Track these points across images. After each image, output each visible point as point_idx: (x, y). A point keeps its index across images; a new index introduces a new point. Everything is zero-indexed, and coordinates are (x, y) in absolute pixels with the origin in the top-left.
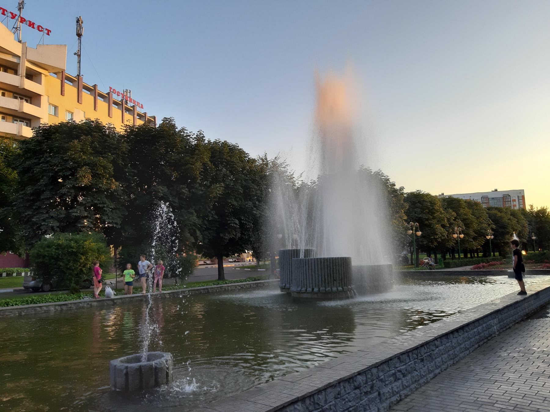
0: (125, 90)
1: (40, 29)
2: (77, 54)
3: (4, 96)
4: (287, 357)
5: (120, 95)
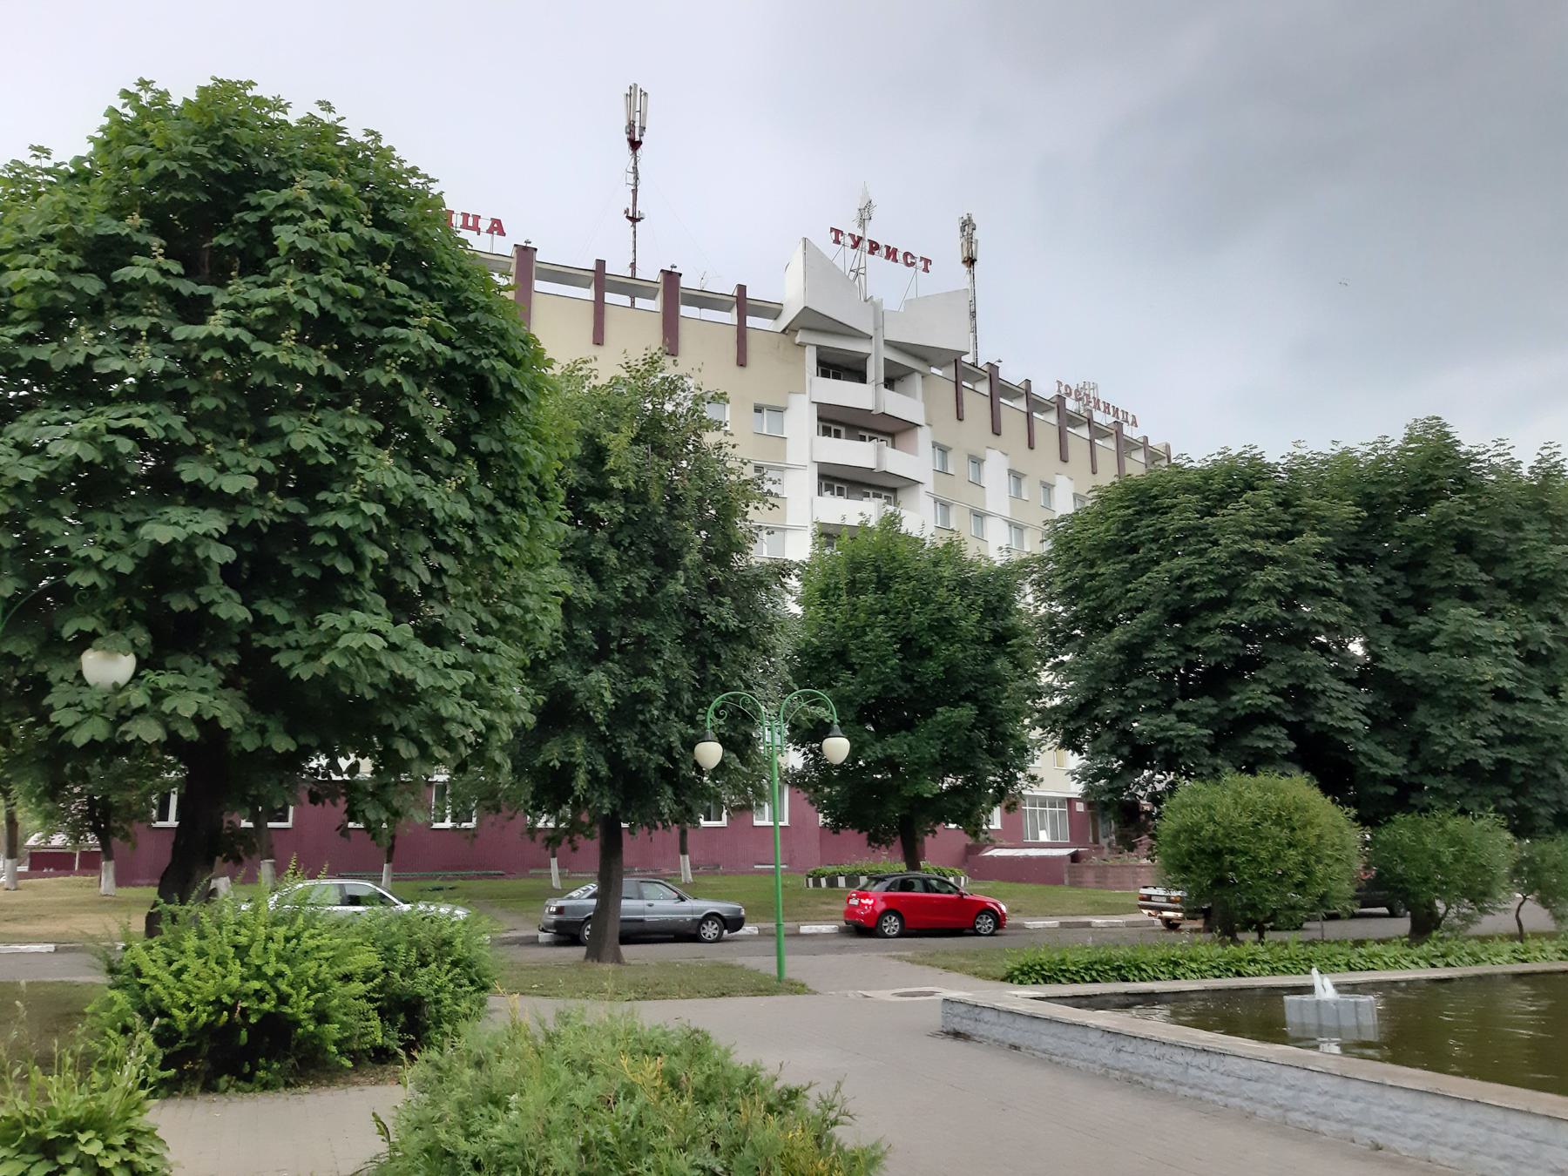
4: (504, 944)
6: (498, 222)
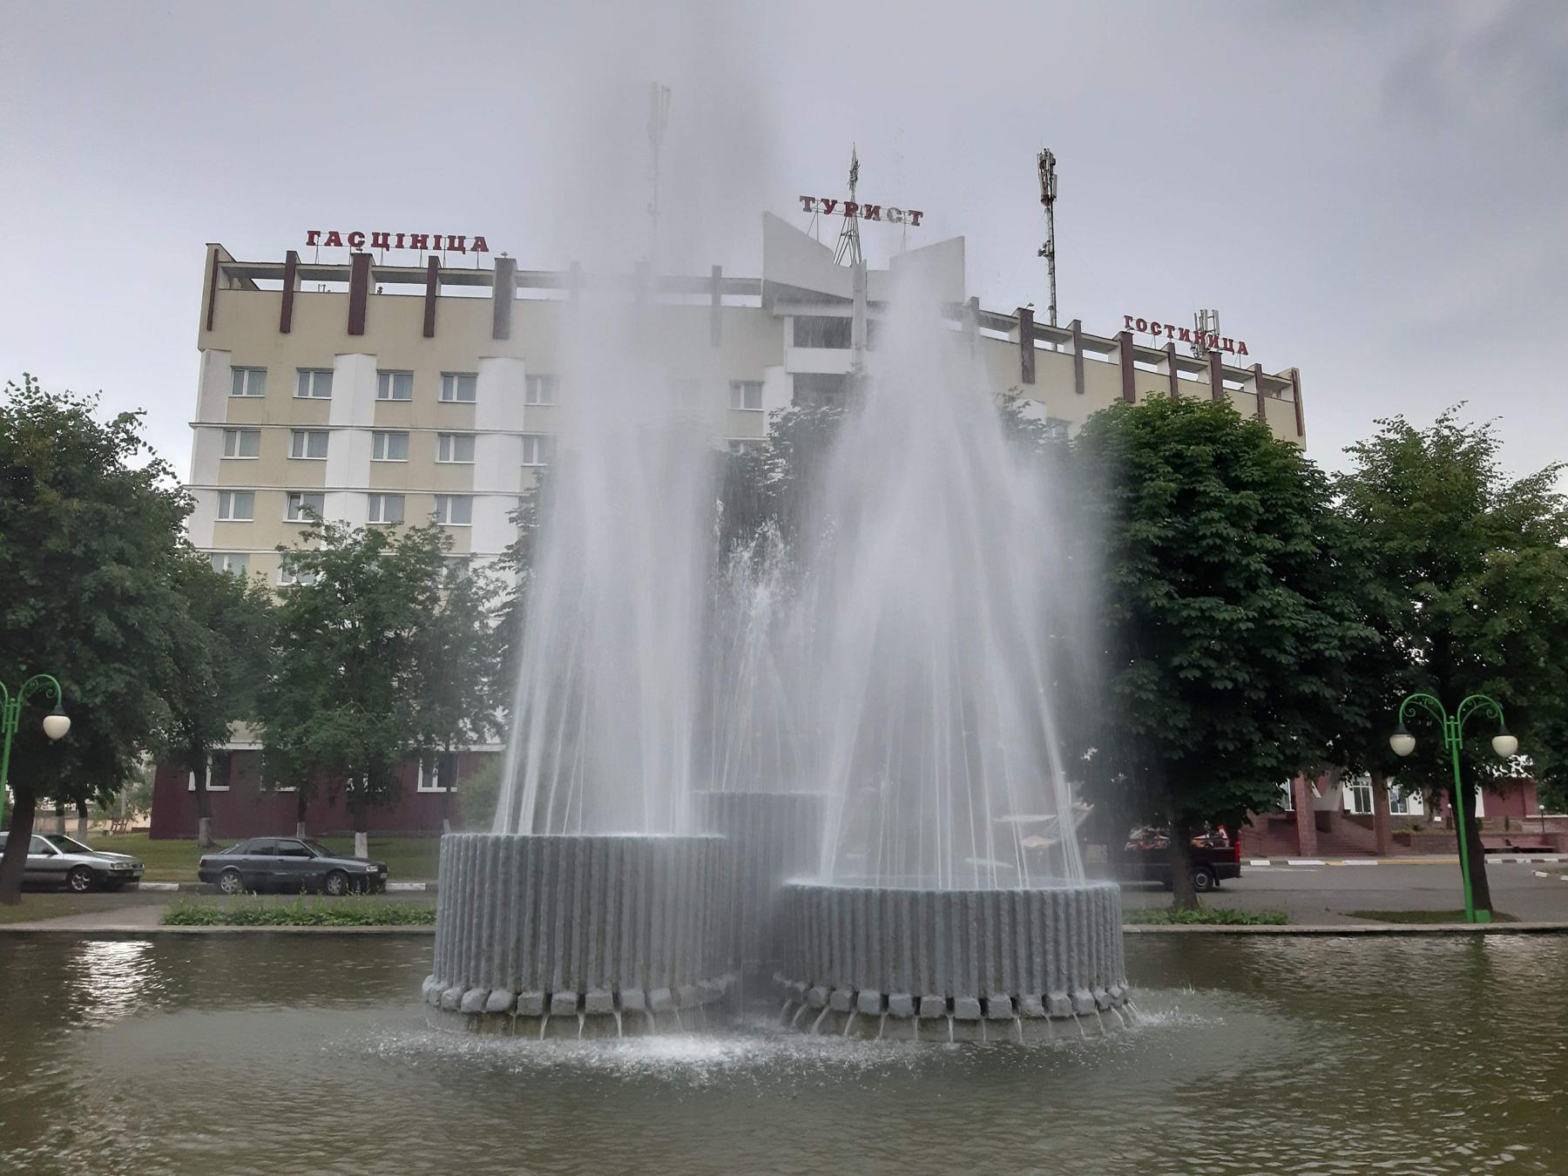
0: (1199, 315)
1: (895, 215)
2: (1044, 252)
3: (333, 370)
5: (1160, 332)
6: (482, 239)
